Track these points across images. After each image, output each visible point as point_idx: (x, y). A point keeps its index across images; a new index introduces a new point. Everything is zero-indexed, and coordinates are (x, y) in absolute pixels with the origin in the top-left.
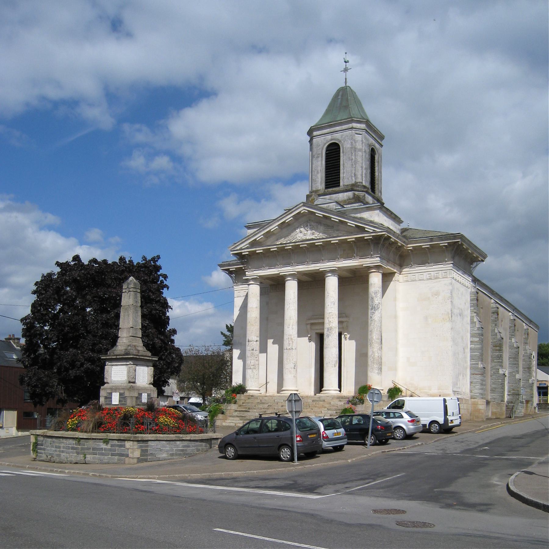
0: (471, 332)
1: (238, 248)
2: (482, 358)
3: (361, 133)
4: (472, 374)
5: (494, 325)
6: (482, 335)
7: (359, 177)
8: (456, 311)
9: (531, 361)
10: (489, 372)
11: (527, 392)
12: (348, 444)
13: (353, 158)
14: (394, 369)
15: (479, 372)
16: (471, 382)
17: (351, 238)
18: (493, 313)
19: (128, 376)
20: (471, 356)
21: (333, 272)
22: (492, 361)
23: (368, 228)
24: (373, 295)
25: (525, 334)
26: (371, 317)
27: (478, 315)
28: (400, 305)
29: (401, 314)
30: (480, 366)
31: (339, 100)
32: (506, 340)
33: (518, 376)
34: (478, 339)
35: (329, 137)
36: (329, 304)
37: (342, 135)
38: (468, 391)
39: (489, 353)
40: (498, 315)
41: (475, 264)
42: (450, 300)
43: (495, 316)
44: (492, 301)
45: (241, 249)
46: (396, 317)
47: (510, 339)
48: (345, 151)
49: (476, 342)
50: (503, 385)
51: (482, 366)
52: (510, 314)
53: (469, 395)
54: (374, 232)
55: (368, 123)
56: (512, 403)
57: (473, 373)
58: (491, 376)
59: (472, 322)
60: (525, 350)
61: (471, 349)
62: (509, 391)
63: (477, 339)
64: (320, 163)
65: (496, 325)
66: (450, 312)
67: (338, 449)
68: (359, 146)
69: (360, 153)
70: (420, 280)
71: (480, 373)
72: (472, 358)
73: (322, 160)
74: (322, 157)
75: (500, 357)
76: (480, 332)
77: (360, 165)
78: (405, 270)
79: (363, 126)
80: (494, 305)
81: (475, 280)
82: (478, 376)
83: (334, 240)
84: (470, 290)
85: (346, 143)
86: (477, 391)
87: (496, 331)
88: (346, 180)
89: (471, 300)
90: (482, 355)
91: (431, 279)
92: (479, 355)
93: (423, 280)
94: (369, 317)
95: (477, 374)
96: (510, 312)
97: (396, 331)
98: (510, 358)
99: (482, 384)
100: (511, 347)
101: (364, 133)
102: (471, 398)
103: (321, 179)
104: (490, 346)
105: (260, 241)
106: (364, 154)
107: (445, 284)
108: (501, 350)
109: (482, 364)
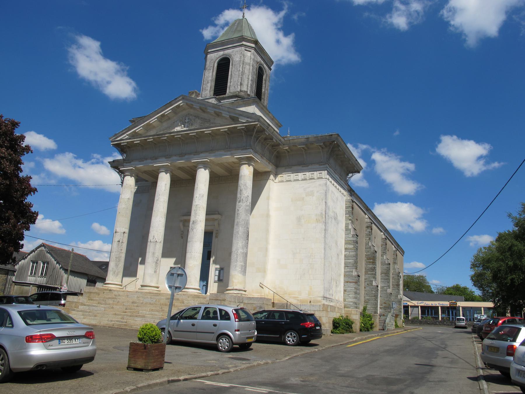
0: (345, 239)
1: (118, 139)
2: (356, 265)
3: (250, 50)
4: (346, 282)
5: (368, 239)
6: (357, 243)
7: (245, 83)
9: (399, 279)
10: (363, 278)
12: (259, 340)
13: (241, 70)
14: (263, 271)
15: (353, 280)
16: (345, 291)
18: (367, 227)
19: (277, 303)
20: (345, 264)
21: (205, 165)
22: (366, 273)
24: (242, 187)
25: (394, 254)
26: (238, 210)
27: (353, 222)
28: (273, 205)
29: (273, 214)
30: (355, 273)
32: (379, 255)
33: (389, 291)
34: (352, 246)
35: (221, 53)
36: (198, 196)
37: (233, 51)
38: (341, 299)
39: (363, 264)
40: (372, 229)
41: (350, 175)
42: (324, 201)
43: (369, 230)
44: (367, 216)
46: (268, 216)
47: (382, 256)
48: (234, 64)
49: (351, 249)
50: (376, 296)
51: (356, 273)
52: (382, 233)
53: (343, 306)
55: (256, 42)
56: (384, 315)
57: (346, 280)
58: (365, 287)
59: (347, 229)
60: (394, 269)
61: (345, 256)
62: (381, 305)
63: (352, 246)
64: (211, 74)
65: (370, 239)
66: (324, 213)
67: (244, 347)
68: (247, 60)
69: (248, 67)
70: (295, 180)
71: (353, 281)
72: (346, 265)
73: (213, 71)
74: (213, 69)
75: (374, 269)
76: (355, 239)
77: (247, 76)
78: (284, 176)
79: (253, 45)
80: (368, 220)
81: (351, 191)
82: (352, 284)
83: (207, 131)
84: (345, 198)
86: (351, 300)
87: (370, 244)
88: (231, 88)
89: (346, 208)
90: (356, 262)
91: (305, 179)
92: (352, 263)
94: (236, 210)
95: (351, 282)
96: (382, 231)
97: (267, 231)
98: (381, 273)
99: (356, 293)
100: (383, 263)
101: (253, 51)
102: (345, 307)
103: (211, 88)
104: (364, 258)
105: (140, 132)
106: (251, 68)
107: (320, 185)
108: (374, 263)
109: (356, 271)
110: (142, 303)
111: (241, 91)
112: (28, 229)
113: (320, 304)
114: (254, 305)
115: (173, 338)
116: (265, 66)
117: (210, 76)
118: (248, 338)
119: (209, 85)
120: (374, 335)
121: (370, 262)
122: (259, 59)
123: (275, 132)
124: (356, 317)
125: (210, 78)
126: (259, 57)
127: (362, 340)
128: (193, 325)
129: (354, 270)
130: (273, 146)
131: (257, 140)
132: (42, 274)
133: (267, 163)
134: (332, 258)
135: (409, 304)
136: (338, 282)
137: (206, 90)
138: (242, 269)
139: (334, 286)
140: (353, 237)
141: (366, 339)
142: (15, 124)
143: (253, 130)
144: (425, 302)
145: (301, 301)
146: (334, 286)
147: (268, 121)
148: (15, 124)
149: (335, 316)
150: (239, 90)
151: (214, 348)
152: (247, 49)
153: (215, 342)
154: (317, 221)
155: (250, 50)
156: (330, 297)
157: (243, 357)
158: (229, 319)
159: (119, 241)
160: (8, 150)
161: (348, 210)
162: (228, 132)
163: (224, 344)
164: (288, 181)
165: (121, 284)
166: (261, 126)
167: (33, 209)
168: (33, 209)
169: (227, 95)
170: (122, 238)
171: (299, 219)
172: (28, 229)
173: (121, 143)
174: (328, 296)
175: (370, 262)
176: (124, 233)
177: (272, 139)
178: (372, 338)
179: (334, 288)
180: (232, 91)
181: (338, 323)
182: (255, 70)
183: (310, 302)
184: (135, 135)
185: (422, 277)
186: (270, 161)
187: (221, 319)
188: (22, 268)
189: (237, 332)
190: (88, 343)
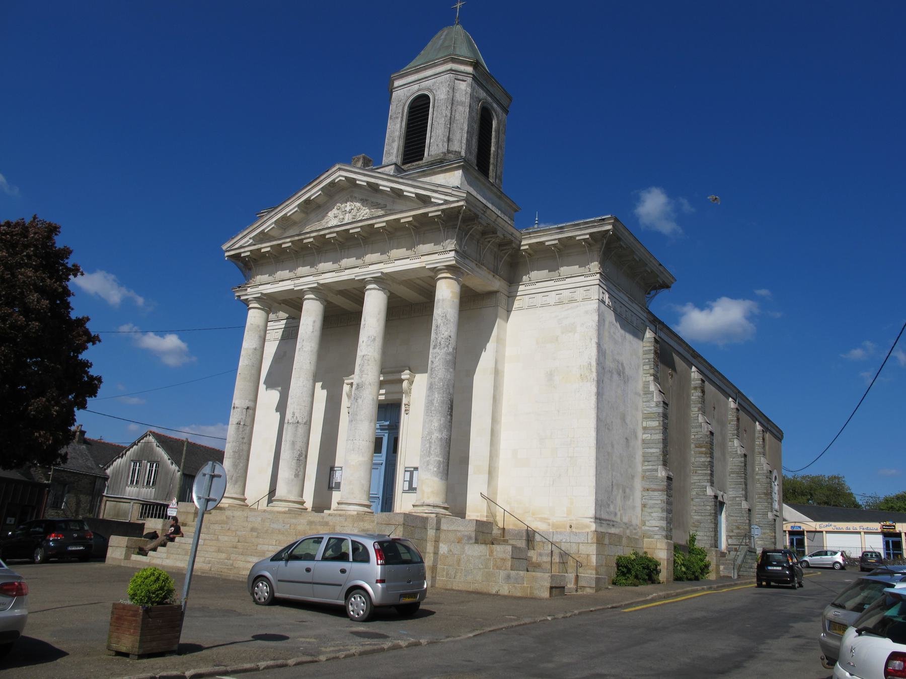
1: (237, 246)
3: (464, 78)
8: (609, 364)
11: (764, 533)
17: (406, 217)
23: (437, 198)
31: (441, 41)
35: (416, 87)
37: (435, 83)
45: (241, 247)
49: (653, 428)
54: (446, 202)
57: (647, 486)
64: (398, 126)
69: (461, 108)
71: (660, 488)
73: (402, 120)
82: (656, 493)
83: (380, 224)
85: (439, 93)
93: (548, 305)
107: (587, 312)
110: (266, 532)
111: (449, 152)
112: (83, 406)
113: (588, 530)
114: (459, 534)
115: (277, 595)
116: (495, 105)
117: (396, 129)
118: (403, 596)
119: (395, 145)
120: (699, 588)
121: (701, 453)
122: (482, 94)
123: (499, 220)
124: (661, 552)
125: (397, 134)
126: (481, 91)
127: (665, 598)
128: (308, 570)
129: (660, 468)
130: (500, 245)
131: (466, 235)
132: (148, 482)
133: (490, 277)
134: (613, 446)
135: (804, 527)
136: (627, 490)
137: (389, 154)
138: (439, 468)
139: (619, 498)
140: (657, 406)
141: (677, 595)
142: (53, 230)
143: (458, 217)
144: (833, 524)
145: (554, 525)
146: (619, 498)
147: (484, 201)
148: (53, 230)
149: (621, 554)
150: (445, 150)
151: (340, 611)
152: (460, 77)
153: (342, 602)
154: (582, 377)
155: (464, 78)
156: (612, 517)
157: (377, 631)
158: (366, 559)
159: (239, 424)
160: (36, 271)
161: (647, 356)
162: (415, 224)
163: (357, 606)
164: (530, 307)
165: (299, 499)
166: (470, 210)
167: (93, 372)
168: (93, 372)
169: (424, 160)
170: (244, 417)
171: (550, 376)
172: (83, 406)
173: (240, 253)
174: (604, 516)
175: (701, 453)
176: (248, 408)
177: (494, 232)
178: (693, 595)
179: (619, 501)
180: (432, 153)
181: (626, 567)
182: (474, 114)
183: (571, 527)
184: (263, 237)
185: (838, 478)
186: (495, 272)
187: (355, 560)
188: (117, 472)
189: (379, 585)
190: (4, 604)
